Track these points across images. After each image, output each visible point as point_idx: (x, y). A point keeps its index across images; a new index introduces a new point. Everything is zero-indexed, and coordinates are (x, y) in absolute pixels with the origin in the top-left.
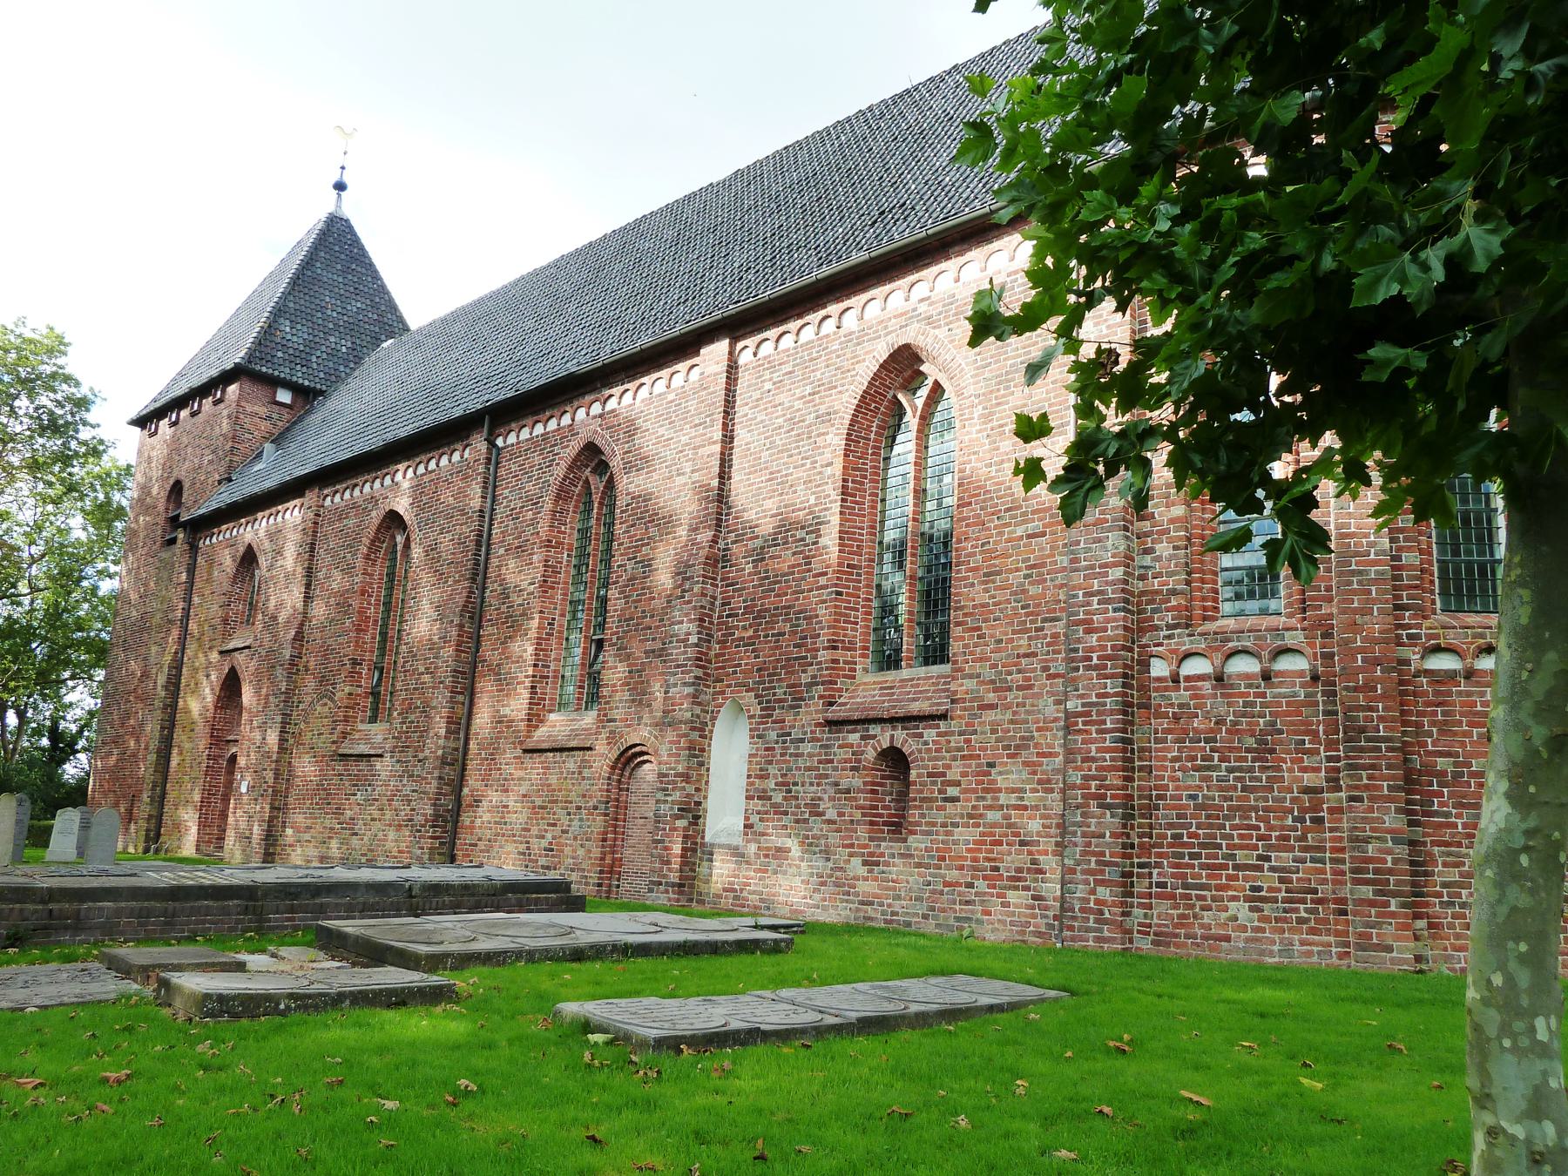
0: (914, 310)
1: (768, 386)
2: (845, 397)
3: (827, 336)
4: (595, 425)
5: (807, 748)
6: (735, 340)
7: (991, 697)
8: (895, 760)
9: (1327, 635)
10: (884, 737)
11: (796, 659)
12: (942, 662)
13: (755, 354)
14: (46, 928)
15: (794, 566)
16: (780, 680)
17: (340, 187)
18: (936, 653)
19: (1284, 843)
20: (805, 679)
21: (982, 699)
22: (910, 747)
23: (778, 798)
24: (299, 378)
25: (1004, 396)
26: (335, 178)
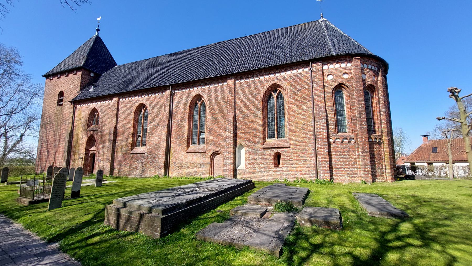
5: (258, 152)
6: (119, 98)
7: (298, 144)
9: (357, 136)
10: (276, 150)
14: (466, 239)
19: (352, 167)
23: (253, 161)
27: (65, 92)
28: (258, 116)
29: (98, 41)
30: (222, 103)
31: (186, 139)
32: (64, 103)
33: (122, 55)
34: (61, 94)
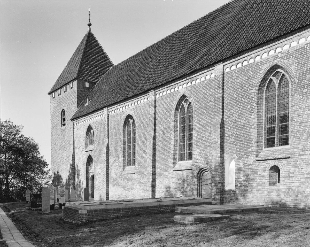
0: (277, 55)
1: (234, 78)
2: (257, 80)
3: (251, 63)
4: (184, 90)
8: (275, 169)
10: (272, 163)
11: (247, 146)
12: (286, 144)
13: (230, 69)
15: (245, 123)
16: (243, 151)
17: (90, 25)
18: (284, 142)
20: (250, 150)
21: (300, 153)
22: (280, 166)
24: (90, 79)
25: (304, 77)
26: (88, 23)
27: (66, 110)
28: (252, 117)
29: (90, 38)
30: (210, 103)
31: (173, 155)
32: (66, 122)
33: (119, 51)
34: (63, 113)
